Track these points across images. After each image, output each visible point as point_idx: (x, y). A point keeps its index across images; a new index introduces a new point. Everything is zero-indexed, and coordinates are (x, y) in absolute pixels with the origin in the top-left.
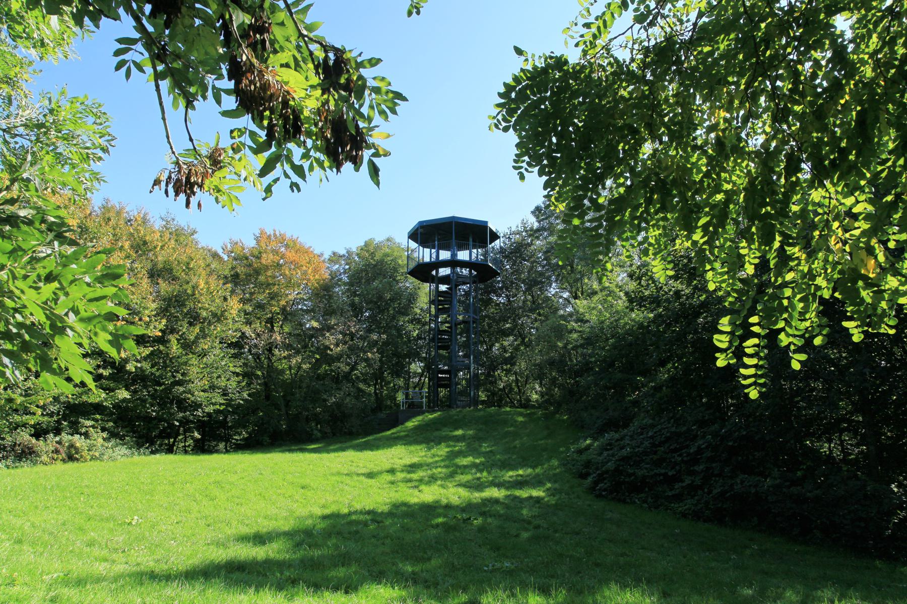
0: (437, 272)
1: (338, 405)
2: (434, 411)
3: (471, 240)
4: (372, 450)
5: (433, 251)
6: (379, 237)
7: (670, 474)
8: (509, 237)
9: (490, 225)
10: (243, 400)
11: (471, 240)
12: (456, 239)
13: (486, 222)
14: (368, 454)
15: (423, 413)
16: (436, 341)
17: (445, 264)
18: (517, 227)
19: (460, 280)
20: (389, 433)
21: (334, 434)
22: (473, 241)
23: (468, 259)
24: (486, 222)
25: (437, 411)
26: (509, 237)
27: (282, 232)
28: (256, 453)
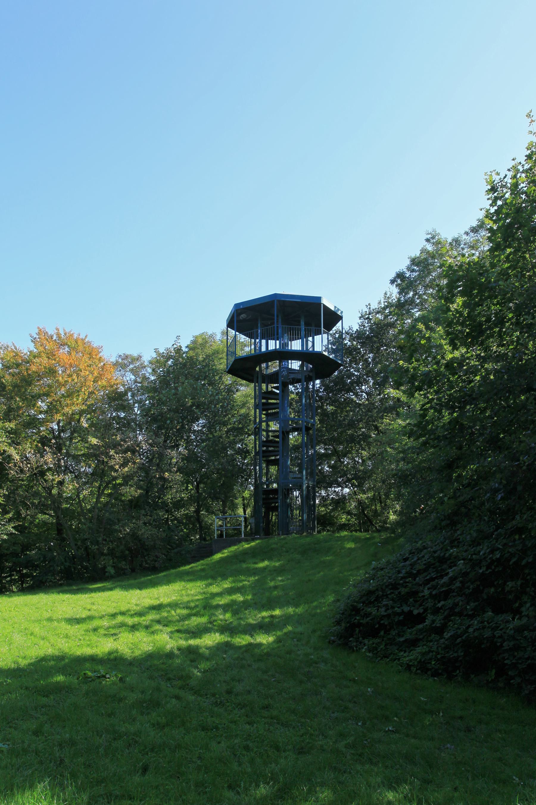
1: (134, 535)
2: (253, 540)
3: (302, 323)
4: (140, 589)
6: (197, 333)
7: (415, 612)
8: (368, 318)
9: (325, 302)
10: (7, 534)
11: (302, 323)
13: (319, 298)
14: (145, 592)
15: (240, 541)
17: (271, 356)
18: (380, 303)
20: (187, 567)
21: (133, 570)
22: (307, 324)
24: (319, 298)
25: (257, 539)
26: (368, 318)
27: (67, 331)
28: (26, 595)
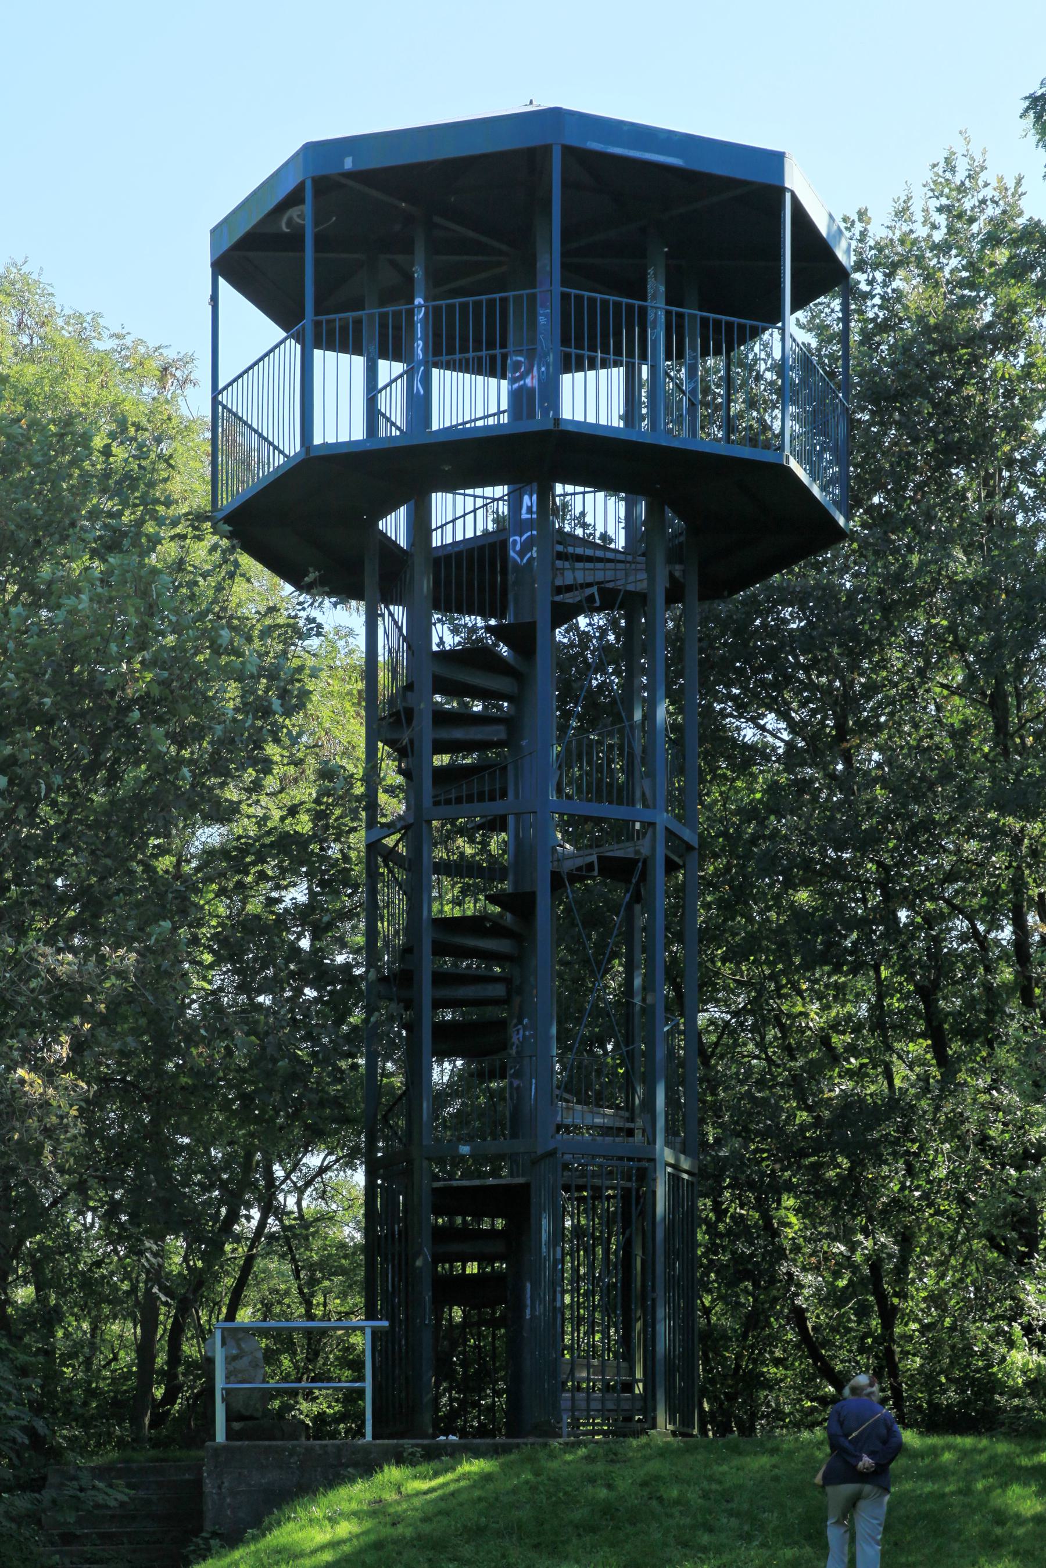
0: (420, 525)
3: (656, 287)
5: (388, 369)
11: (656, 287)
12: (572, 272)
13: (776, 159)
15: (367, 1467)
16: (427, 992)
18: (902, 213)
19: (578, 574)
23: (359, 434)
24: (776, 159)
25: (455, 1453)
